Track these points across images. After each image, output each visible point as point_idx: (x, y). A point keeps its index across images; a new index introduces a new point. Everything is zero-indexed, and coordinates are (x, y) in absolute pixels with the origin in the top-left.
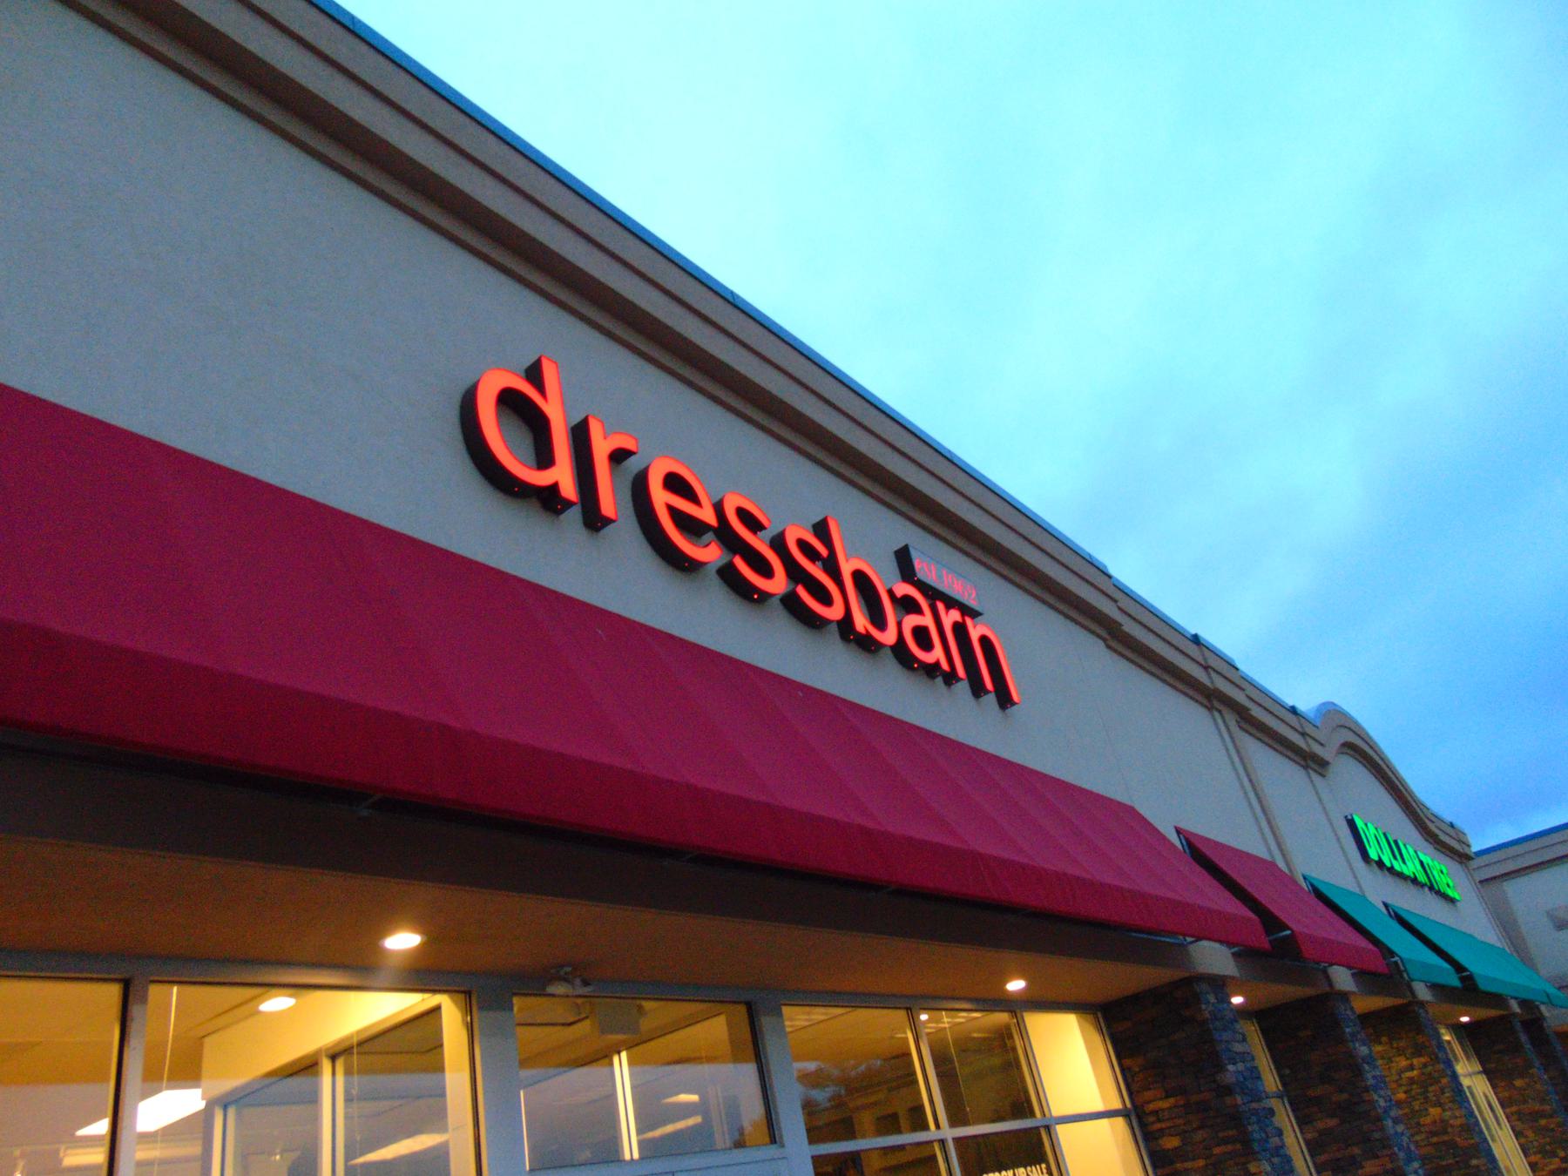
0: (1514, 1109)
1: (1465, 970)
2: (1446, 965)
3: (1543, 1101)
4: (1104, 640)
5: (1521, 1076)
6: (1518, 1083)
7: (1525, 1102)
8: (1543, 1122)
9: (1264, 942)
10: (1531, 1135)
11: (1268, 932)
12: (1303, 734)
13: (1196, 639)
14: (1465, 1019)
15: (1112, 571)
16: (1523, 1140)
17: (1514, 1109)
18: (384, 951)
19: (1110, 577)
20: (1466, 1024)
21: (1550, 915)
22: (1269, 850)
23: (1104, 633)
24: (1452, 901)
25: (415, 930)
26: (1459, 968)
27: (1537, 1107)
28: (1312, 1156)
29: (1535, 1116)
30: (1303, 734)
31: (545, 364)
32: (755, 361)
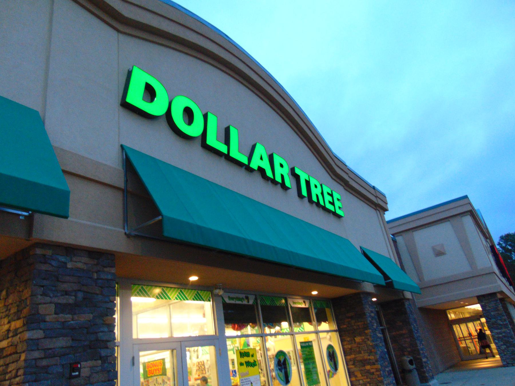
0: (353, 356)
1: (389, 279)
2: (380, 274)
3: (370, 353)
4: (343, 187)
5: (360, 335)
6: (358, 339)
7: (360, 352)
8: (368, 367)
9: (383, 282)
10: (359, 375)
11: (385, 280)
12: (376, 197)
13: (374, 188)
14: (315, 293)
15: (347, 164)
16: (353, 379)
17: (353, 356)
18: (189, 281)
19: (346, 166)
20: (193, 282)
21: (434, 249)
22: (390, 256)
23: (343, 184)
24: (339, 217)
25: (198, 276)
26: (386, 277)
27: (366, 357)
28: (345, 356)
29: (364, 362)
30: (376, 197)
31: (231, 127)
32: (140, 11)
